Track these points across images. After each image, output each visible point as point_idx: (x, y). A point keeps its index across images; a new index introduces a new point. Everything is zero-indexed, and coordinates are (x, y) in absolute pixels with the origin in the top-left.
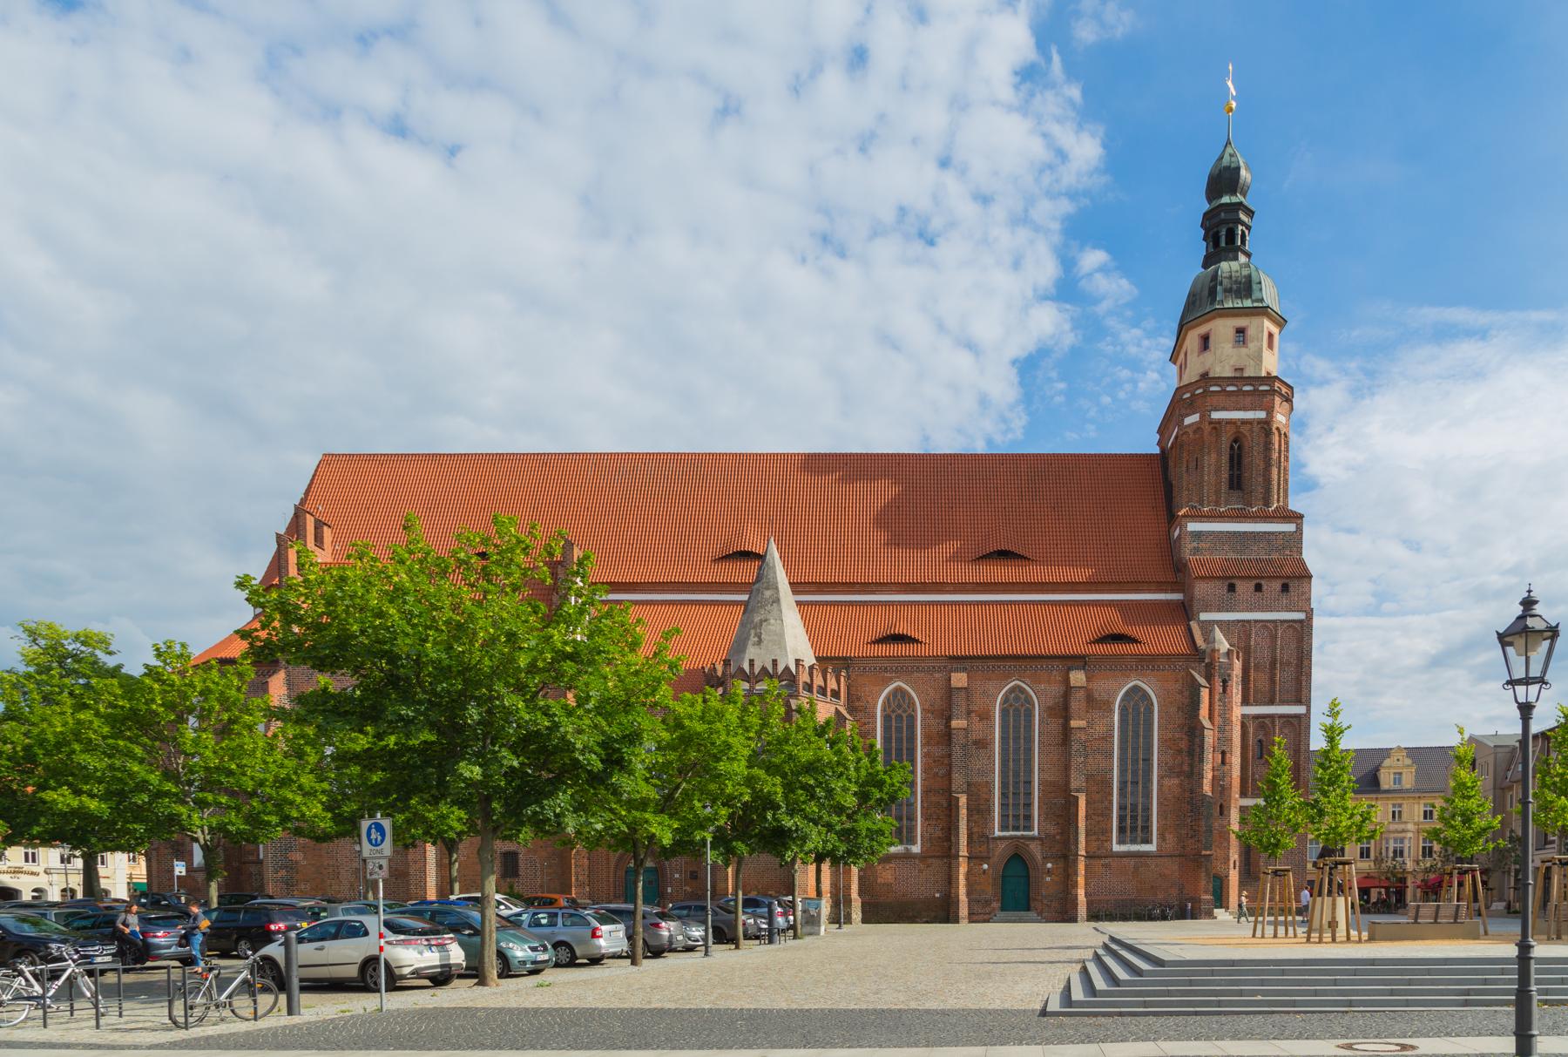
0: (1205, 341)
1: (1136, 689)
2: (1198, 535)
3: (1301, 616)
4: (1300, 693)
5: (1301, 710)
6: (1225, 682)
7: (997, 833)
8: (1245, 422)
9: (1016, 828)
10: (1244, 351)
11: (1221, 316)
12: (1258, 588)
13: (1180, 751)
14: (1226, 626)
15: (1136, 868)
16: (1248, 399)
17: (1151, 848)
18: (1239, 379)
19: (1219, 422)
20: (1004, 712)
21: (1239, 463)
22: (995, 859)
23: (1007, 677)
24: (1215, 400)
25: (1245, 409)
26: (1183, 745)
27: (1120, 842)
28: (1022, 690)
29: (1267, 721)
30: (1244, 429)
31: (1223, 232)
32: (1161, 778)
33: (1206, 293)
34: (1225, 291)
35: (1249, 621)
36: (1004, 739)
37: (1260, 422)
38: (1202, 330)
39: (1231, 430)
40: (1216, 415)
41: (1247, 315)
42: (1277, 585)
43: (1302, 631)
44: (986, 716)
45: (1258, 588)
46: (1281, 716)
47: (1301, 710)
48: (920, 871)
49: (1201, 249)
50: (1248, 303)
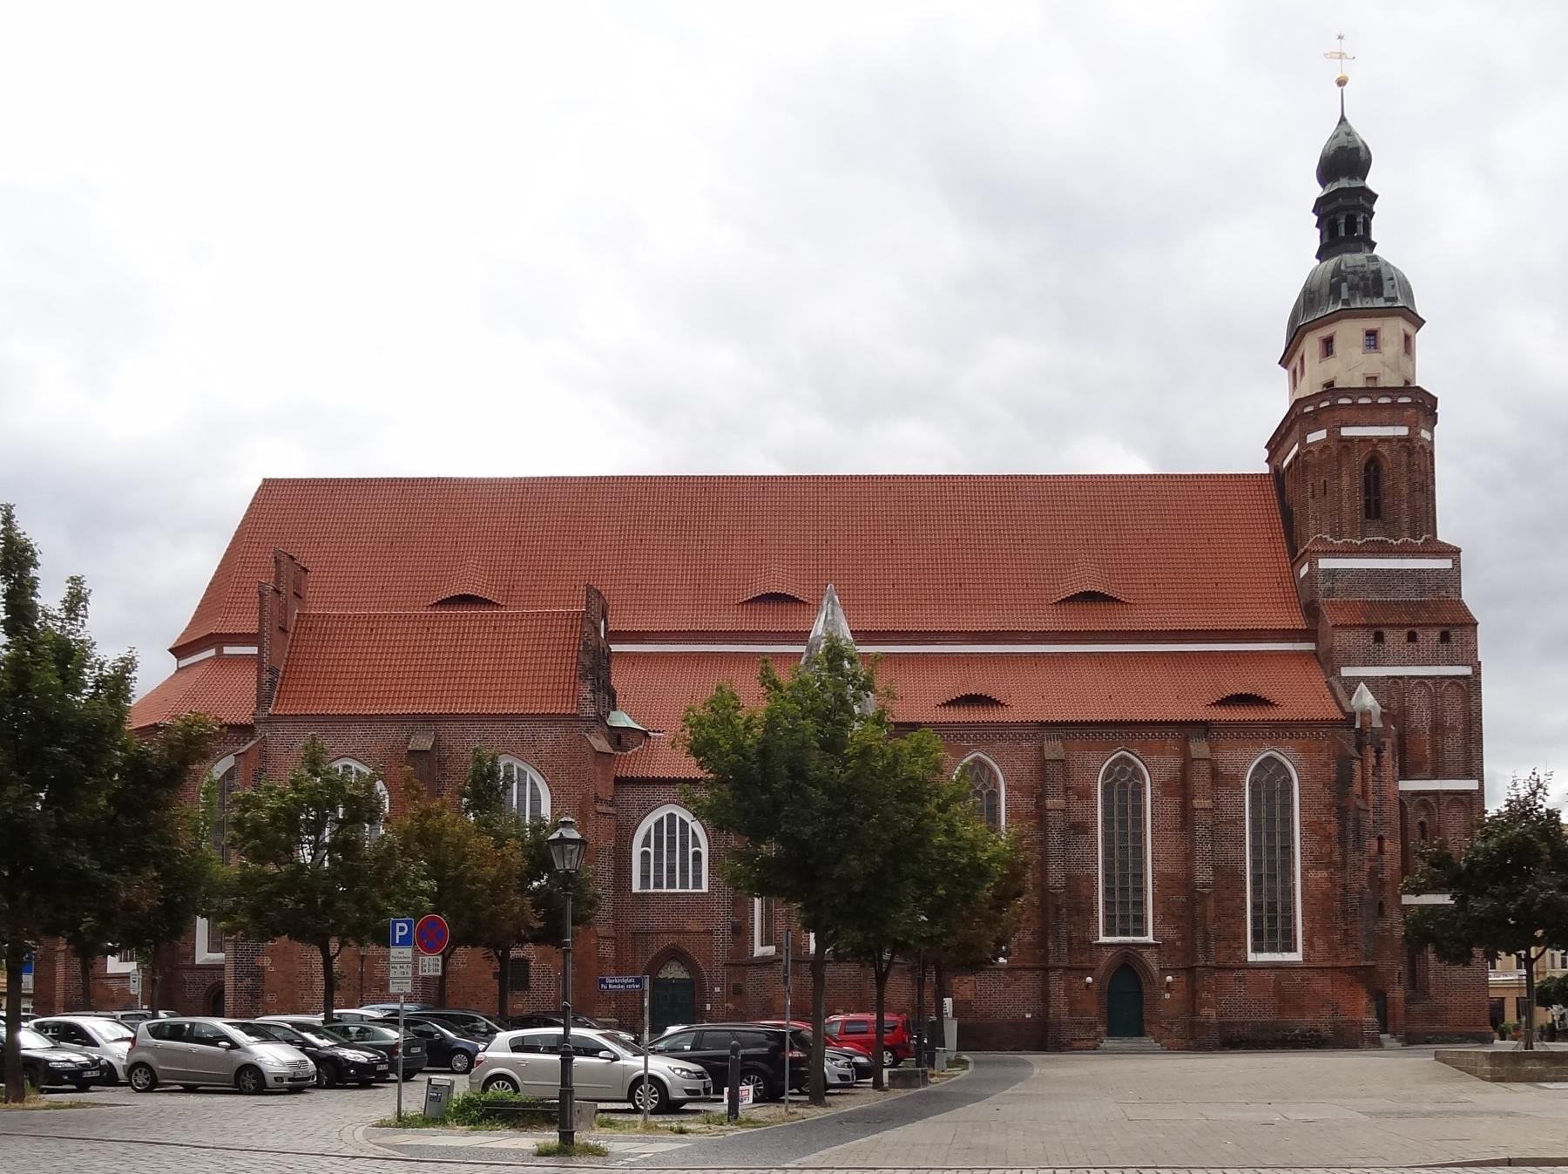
0: (1328, 346)
1: (977, 761)
2: (1332, 574)
3: (1467, 671)
4: (1473, 768)
5: (1472, 785)
6: (1378, 752)
7: (1103, 939)
8: (1382, 440)
9: (1125, 933)
10: (1376, 357)
11: (1348, 317)
12: (1412, 637)
13: (1328, 838)
14: (1367, 680)
15: (1277, 982)
16: (1386, 414)
17: (1296, 957)
18: (1373, 389)
19: (1351, 439)
20: (1107, 789)
21: (1367, 481)
22: (1101, 971)
23: (1110, 747)
24: (1345, 415)
25: (1382, 425)
26: (1333, 829)
27: (1108, 933)
28: (1129, 762)
29: (1430, 799)
30: (1384, 449)
31: (1345, 207)
32: (1305, 870)
33: (1326, 290)
34: (1350, 288)
35: (1401, 677)
36: (1107, 823)
37: (1400, 439)
38: (1325, 332)
39: (1360, 458)
40: (1346, 432)
41: (1379, 316)
42: (1435, 635)
43: (1470, 688)
44: (1086, 794)
45: (1412, 637)
46: (1448, 793)
47: (1472, 785)
48: (1007, 986)
49: (1313, 239)
50: (1380, 303)
